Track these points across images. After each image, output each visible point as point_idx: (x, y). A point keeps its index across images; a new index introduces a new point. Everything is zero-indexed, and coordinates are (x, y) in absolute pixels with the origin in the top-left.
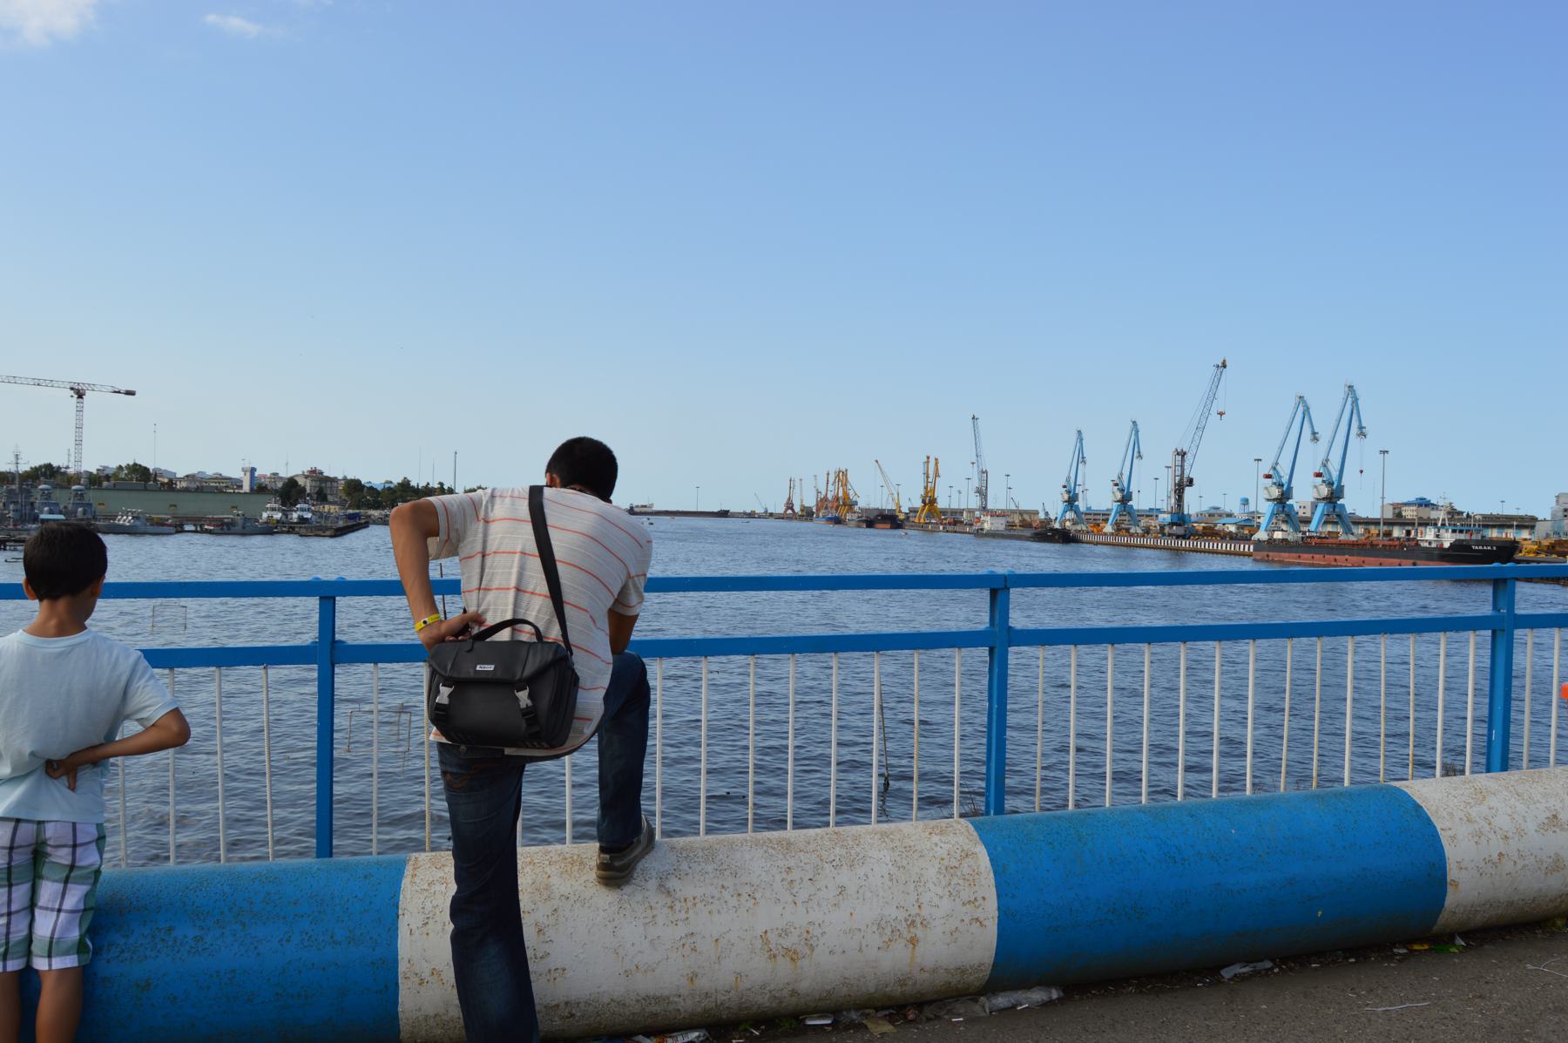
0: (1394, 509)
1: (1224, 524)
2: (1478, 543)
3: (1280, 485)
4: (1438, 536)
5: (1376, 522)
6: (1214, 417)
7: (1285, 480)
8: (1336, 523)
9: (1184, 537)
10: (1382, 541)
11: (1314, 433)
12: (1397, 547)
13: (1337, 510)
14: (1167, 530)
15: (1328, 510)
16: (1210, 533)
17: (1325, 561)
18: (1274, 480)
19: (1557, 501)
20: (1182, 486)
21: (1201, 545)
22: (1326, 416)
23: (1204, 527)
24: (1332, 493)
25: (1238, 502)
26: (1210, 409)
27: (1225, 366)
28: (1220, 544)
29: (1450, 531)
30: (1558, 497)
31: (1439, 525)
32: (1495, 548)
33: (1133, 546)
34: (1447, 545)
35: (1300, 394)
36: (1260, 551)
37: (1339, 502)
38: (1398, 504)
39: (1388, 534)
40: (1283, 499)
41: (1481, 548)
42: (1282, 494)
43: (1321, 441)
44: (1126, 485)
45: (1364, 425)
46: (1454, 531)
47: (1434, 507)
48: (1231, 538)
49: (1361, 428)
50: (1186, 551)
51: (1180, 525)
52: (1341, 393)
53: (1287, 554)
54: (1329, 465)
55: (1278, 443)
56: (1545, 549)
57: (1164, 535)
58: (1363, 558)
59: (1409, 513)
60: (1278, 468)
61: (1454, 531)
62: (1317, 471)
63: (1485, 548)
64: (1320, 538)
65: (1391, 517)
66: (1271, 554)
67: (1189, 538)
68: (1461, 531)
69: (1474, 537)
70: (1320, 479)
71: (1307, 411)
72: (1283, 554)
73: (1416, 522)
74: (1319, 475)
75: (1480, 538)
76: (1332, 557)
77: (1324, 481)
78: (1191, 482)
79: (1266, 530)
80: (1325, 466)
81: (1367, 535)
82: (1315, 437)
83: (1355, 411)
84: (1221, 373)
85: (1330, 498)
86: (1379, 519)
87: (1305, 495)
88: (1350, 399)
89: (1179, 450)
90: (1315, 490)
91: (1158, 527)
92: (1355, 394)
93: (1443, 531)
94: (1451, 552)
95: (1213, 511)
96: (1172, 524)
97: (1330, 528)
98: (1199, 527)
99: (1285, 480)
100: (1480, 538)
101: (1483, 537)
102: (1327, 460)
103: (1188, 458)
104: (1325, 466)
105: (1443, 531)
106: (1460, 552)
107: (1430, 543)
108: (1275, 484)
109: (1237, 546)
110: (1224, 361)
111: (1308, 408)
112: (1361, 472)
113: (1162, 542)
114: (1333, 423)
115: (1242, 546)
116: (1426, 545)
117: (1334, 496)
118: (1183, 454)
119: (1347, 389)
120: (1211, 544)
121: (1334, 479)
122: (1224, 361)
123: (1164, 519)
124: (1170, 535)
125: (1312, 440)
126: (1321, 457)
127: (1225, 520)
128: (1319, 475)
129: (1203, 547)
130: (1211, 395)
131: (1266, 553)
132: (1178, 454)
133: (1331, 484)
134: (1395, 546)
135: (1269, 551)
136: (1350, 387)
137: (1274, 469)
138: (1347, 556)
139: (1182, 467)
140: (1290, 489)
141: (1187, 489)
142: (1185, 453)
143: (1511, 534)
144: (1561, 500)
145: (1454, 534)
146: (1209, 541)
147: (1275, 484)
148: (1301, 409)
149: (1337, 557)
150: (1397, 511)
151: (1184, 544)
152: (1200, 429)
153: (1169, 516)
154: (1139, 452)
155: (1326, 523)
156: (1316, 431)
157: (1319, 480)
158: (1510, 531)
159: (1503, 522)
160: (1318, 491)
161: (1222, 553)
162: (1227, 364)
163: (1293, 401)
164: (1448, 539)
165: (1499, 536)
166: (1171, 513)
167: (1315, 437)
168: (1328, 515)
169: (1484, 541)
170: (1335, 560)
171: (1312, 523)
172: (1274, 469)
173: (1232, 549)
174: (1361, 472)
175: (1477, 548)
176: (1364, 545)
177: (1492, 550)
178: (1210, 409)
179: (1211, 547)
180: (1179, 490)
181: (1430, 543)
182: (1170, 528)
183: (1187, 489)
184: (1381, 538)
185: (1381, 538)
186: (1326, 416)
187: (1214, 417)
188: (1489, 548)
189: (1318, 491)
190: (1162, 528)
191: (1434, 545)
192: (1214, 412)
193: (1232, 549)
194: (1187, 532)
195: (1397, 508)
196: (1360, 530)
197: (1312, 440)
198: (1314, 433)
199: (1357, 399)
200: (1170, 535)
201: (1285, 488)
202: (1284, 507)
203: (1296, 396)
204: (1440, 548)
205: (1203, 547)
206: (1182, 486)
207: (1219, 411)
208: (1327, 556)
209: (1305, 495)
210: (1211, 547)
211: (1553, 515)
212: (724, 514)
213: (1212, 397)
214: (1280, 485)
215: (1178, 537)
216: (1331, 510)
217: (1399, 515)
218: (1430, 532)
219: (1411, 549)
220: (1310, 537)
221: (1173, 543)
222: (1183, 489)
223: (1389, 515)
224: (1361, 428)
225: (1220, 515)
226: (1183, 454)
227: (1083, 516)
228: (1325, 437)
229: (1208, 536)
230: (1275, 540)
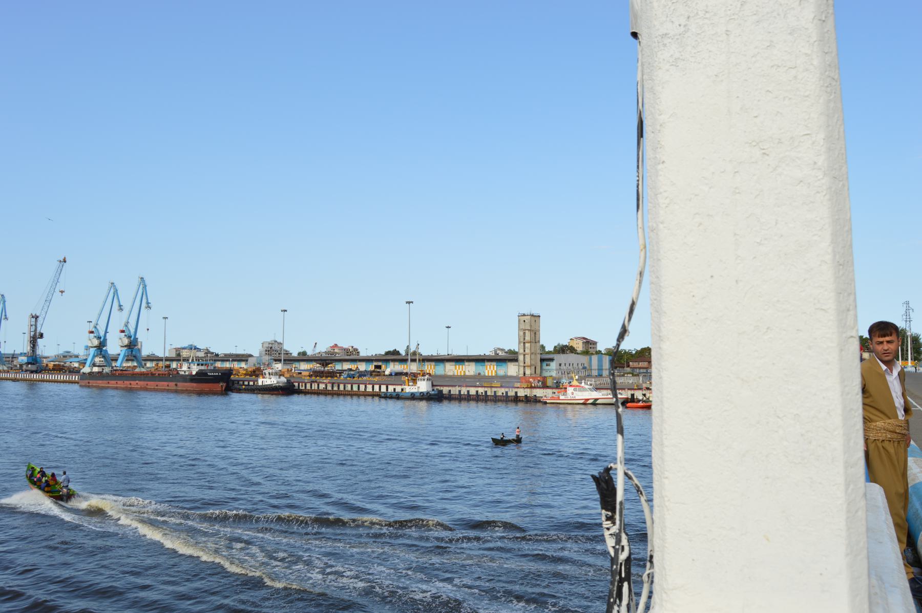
0: (176, 351)
1: (71, 362)
2: (211, 371)
3: (99, 338)
4: (189, 368)
5: (161, 359)
6: (57, 294)
7: (102, 334)
8: (132, 360)
9: (36, 372)
10: (163, 371)
11: (120, 306)
12: (167, 375)
13: (134, 353)
14: (24, 367)
15: (128, 353)
16: (58, 369)
17: (124, 385)
18: (95, 335)
19: (263, 346)
20: (35, 339)
21: (47, 377)
22: (127, 295)
23: (54, 365)
24: (130, 343)
25: (83, 348)
26: (55, 289)
27: (65, 261)
28: (59, 376)
29: (196, 364)
30: (336, 345)
31: (190, 361)
32: (220, 374)
33: (4, 379)
34: (194, 373)
35: (141, 276)
36: (83, 380)
37: (104, 349)
38: (179, 348)
39: (168, 366)
40: (101, 347)
41: (212, 374)
42: (100, 344)
43: (124, 310)
44: (132, 331)
45: (121, 304)
46: (198, 365)
47: (199, 350)
48: (70, 372)
49: (148, 303)
50: (39, 381)
51: (34, 364)
52: (136, 281)
53: (101, 382)
54: (129, 326)
55: (98, 312)
56: (250, 373)
57: (22, 371)
58: (146, 383)
59: (185, 354)
60: (98, 327)
61: (198, 365)
62: (91, 330)
63: (215, 374)
64: (122, 370)
65: (174, 356)
66: (91, 381)
67: (40, 372)
68: (202, 365)
69: (209, 368)
70: (123, 334)
71: (116, 291)
72: (98, 381)
73: (164, 359)
74: (123, 331)
75: (212, 368)
76: (128, 382)
77: (125, 335)
78: (41, 336)
79: (90, 366)
80: (126, 326)
81: (156, 367)
82: (121, 308)
83: (144, 293)
84: (63, 266)
85: (129, 346)
86: (163, 357)
87: (115, 347)
88: (141, 287)
89: (34, 315)
90: (120, 341)
91: (18, 366)
92: (145, 283)
93: (192, 365)
94: (196, 377)
95: (66, 354)
96: (28, 363)
97: (130, 364)
98: (51, 365)
99: (102, 334)
100: (212, 368)
101: (215, 367)
102: (128, 322)
103: (40, 320)
104: (126, 326)
105: (192, 365)
106: (201, 377)
107: (185, 372)
108: (95, 337)
109: (71, 377)
110: (65, 258)
111: (117, 290)
112: (148, 330)
113: (19, 376)
114: (131, 300)
115: (74, 377)
116: (183, 373)
117: (132, 345)
118: (36, 317)
119: (140, 279)
120: (53, 376)
121: (132, 334)
122: (65, 258)
123: (22, 360)
124: (26, 371)
125: (119, 310)
126: (125, 320)
127: (71, 360)
128: (123, 331)
129: (48, 378)
130: (56, 280)
131: (87, 381)
132: (33, 317)
133: (130, 337)
134: (165, 374)
135: (90, 380)
136: (142, 278)
137: (95, 327)
138: (137, 382)
139: (36, 326)
140: (105, 340)
141: (39, 340)
142: (37, 317)
143: (227, 365)
144: (265, 345)
145: (198, 367)
146: (52, 374)
147: (95, 337)
148: (112, 291)
149: (132, 382)
150: (178, 352)
151: (35, 376)
152: (48, 301)
153: (26, 358)
154: (6, 316)
155: (127, 360)
156: (149, 302)
157: (92, 335)
158: (228, 363)
159: (227, 358)
160: (122, 341)
161: (47, 381)
162: (67, 260)
163: (107, 286)
164: (195, 369)
165: (222, 366)
166: (28, 356)
167: (121, 308)
168: (128, 356)
169: (215, 370)
170: (131, 384)
171: (119, 360)
172: (95, 327)
173: (67, 379)
174: (148, 330)
175: (210, 374)
176: (148, 374)
177: (219, 375)
178: (55, 289)
179: (53, 378)
180: (34, 341)
181: (185, 372)
182: (27, 366)
183: (39, 340)
184: (163, 369)
185: (163, 369)
186: (127, 295)
187: (57, 294)
188: (217, 374)
189: (122, 341)
190: (21, 366)
191: (187, 373)
192: (57, 290)
193: (67, 379)
194: (39, 368)
195: (178, 351)
196: (149, 364)
197: (119, 310)
198: (120, 306)
199: (146, 286)
200: (26, 371)
201: (102, 340)
202: (101, 351)
203: (139, 277)
204: (191, 375)
205: (48, 378)
206: (35, 339)
207: (61, 290)
208: (125, 382)
209: (115, 347)
210: (53, 378)
211: (260, 354)
212: (641, 274)
213: (57, 281)
214: (99, 338)
215: (32, 372)
216: (130, 353)
217: (179, 355)
218: (185, 365)
219: (173, 376)
220: (116, 370)
221: (28, 376)
222: (36, 340)
223: (174, 355)
224: (148, 303)
225: (71, 357)
226: (36, 317)
227: (4, 359)
228: (127, 308)
229: (57, 371)
230: (93, 373)
